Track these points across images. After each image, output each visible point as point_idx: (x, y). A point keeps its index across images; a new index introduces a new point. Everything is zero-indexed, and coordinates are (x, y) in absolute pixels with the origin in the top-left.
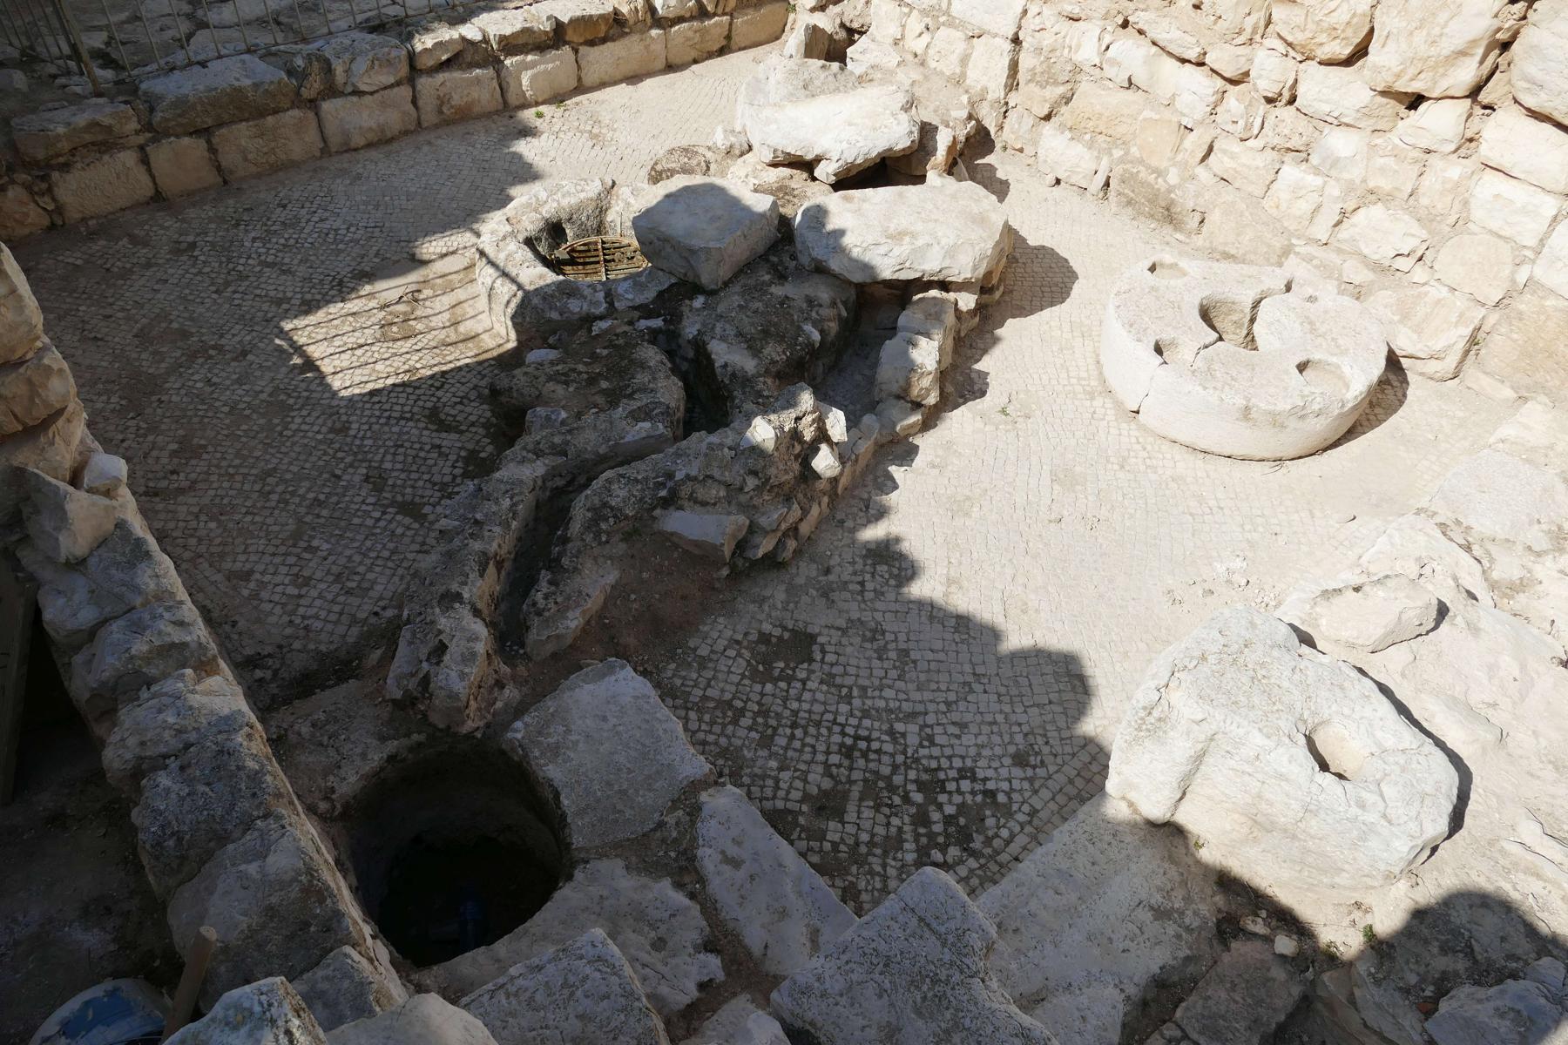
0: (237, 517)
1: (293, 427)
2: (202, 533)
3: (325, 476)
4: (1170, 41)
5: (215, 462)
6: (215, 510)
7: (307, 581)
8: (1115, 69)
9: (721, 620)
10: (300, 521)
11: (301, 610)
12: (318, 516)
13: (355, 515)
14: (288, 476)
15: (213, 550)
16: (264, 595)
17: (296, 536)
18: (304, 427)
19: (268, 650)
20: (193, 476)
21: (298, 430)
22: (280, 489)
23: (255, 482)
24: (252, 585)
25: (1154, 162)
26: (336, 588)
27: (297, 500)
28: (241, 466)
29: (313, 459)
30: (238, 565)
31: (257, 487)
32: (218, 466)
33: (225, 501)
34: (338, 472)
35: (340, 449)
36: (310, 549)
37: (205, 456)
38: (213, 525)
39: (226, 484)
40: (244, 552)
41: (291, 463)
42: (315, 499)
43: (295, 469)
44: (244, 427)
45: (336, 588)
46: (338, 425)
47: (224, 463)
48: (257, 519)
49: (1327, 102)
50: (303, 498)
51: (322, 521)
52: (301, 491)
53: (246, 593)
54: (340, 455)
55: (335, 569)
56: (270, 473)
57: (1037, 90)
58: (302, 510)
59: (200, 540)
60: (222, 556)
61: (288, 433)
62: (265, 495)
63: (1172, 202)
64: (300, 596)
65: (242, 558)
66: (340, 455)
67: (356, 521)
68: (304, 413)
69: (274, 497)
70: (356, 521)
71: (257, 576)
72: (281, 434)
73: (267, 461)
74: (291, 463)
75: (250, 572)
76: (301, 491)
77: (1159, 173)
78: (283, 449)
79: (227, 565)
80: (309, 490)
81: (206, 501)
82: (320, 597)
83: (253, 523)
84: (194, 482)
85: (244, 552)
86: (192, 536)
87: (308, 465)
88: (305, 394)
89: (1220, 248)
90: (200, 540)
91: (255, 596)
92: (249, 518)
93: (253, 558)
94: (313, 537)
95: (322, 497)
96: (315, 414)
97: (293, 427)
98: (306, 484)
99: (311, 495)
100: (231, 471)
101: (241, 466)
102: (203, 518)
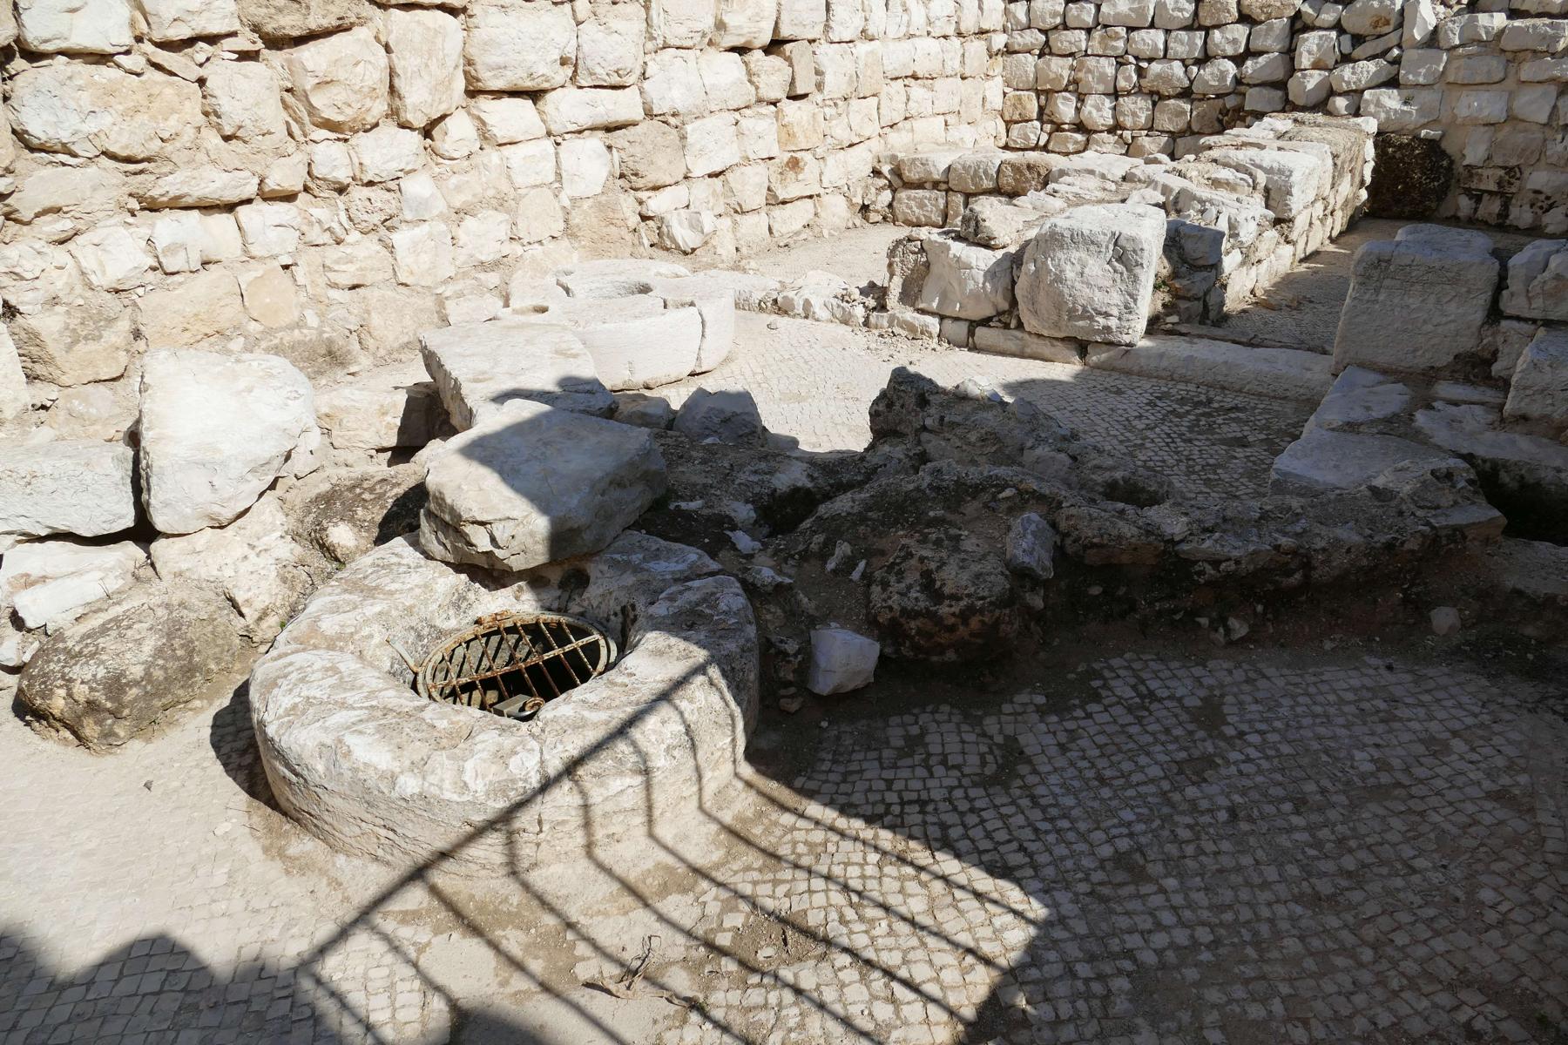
0: (1436, 877)
1: (1181, 936)
2: (1514, 893)
3: (1244, 826)
4: (224, 188)
5: (1378, 993)
6: (1462, 913)
7: (1429, 741)
8: (182, 253)
9: (946, 708)
10: (1353, 806)
11: (1470, 721)
12: (1323, 791)
13: (1280, 755)
14: (1293, 870)
15: (1521, 859)
16: (1500, 762)
17: (1379, 792)
18: (1167, 918)
19: (1549, 717)
20: (1444, 999)
21: (1182, 923)
22: (1328, 866)
23: (1351, 907)
24: (1505, 780)
25: (285, 320)
26: (1403, 712)
27: (1324, 833)
28: (1343, 950)
29: (1227, 862)
30: (1501, 814)
31: (1357, 896)
32: (1381, 981)
33: (1430, 912)
34: (1223, 816)
35: (1175, 839)
36: (1383, 765)
37: (1385, 1019)
38: (1487, 895)
39: (1401, 939)
40: (1476, 823)
41: (1265, 885)
42: (1297, 812)
43: (1271, 873)
44: (1256, 1011)
45: (1403, 712)
46: (1121, 876)
47: (1366, 977)
48: (1407, 852)
49: (392, 159)
50: (1311, 828)
51: (1326, 783)
52: (1303, 837)
53: (1523, 779)
54: (1185, 834)
55: (1380, 728)
56: (1315, 901)
57: (92, 346)
58: (1333, 815)
59: (1528, 887)
60: (1515, 841)
61: (1204, 935)
62: (1356, 878)
63: (330, 341)
64: (1455, 734)
65: (1487, 819)
66: (1185, 834)
67: (1286, 749)
68: (1134, 941)
69: (1349, 863)
70: (1286, 749)
71: (1487, 784)
72: (1216, 943)
73: (1293, 919)
74: (1265, 885)
75: (1489, 795)
76: (1303, 837)
77: (300, 324)
78: (1246, 914)
79: (1521, 826)
80: (1290, 830)
81: (1462, 938)
82: (1431, 718)
83: (1421, 853)
84: (1451, 987)
85: (1476, 823)
86: (1535, 902)
87: (1247, 860)
88: (1083, 970)
89: (396, 345)
90: (1528, 887)
91: (1511, 767)
92: (1420, 863)
93: (1470, 808)
94: (1363, 777)
95: (1287, 807)
96: (1123, 922)
97: (1181, 936)
98: (1283, 840)
99: (1296, 820)
100: (1367, 955)
101: (1343, 950)
102: (1491, 917)
